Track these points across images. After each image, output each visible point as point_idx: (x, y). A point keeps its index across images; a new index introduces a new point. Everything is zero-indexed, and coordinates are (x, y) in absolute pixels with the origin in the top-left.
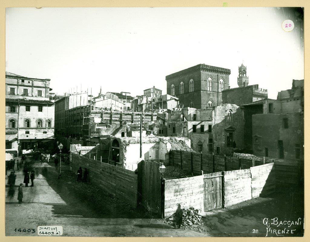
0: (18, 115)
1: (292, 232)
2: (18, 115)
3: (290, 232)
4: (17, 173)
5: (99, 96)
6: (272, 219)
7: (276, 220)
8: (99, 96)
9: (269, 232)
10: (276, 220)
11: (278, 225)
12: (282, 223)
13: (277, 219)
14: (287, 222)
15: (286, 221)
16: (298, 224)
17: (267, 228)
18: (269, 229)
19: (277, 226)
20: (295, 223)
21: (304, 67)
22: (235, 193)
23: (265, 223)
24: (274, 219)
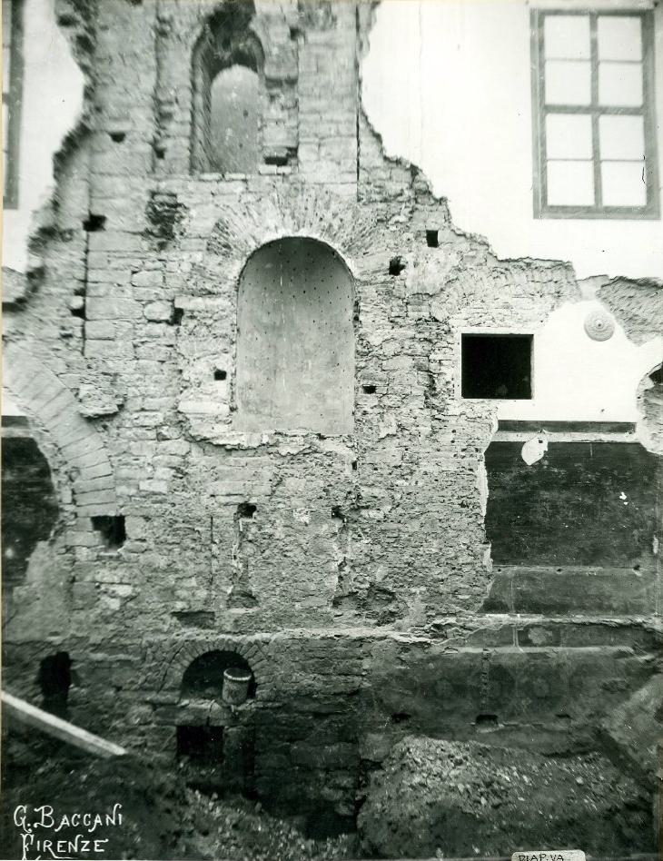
0: (539, 88)
1: (96, 845)
2: (539, 88)
3: (91, 846)
4: (74, 618)
5: (75, 278)
6: (36, 810)
7: (47, 810)
8: (75, 278)
9: (32, 847)
10: (47, 810)
11: (56, 826)
12: (100, 822)
13: (50, 810)
14: (82, 817)
15: (79, 816)
16: (113, 822)
17: (24, 837)
18: (28, 838)
19: (56, 830)
20: (103, 820)
21: (579, 162)
22: (343, 721)
23: (19, 821)
24: (43, 808)
